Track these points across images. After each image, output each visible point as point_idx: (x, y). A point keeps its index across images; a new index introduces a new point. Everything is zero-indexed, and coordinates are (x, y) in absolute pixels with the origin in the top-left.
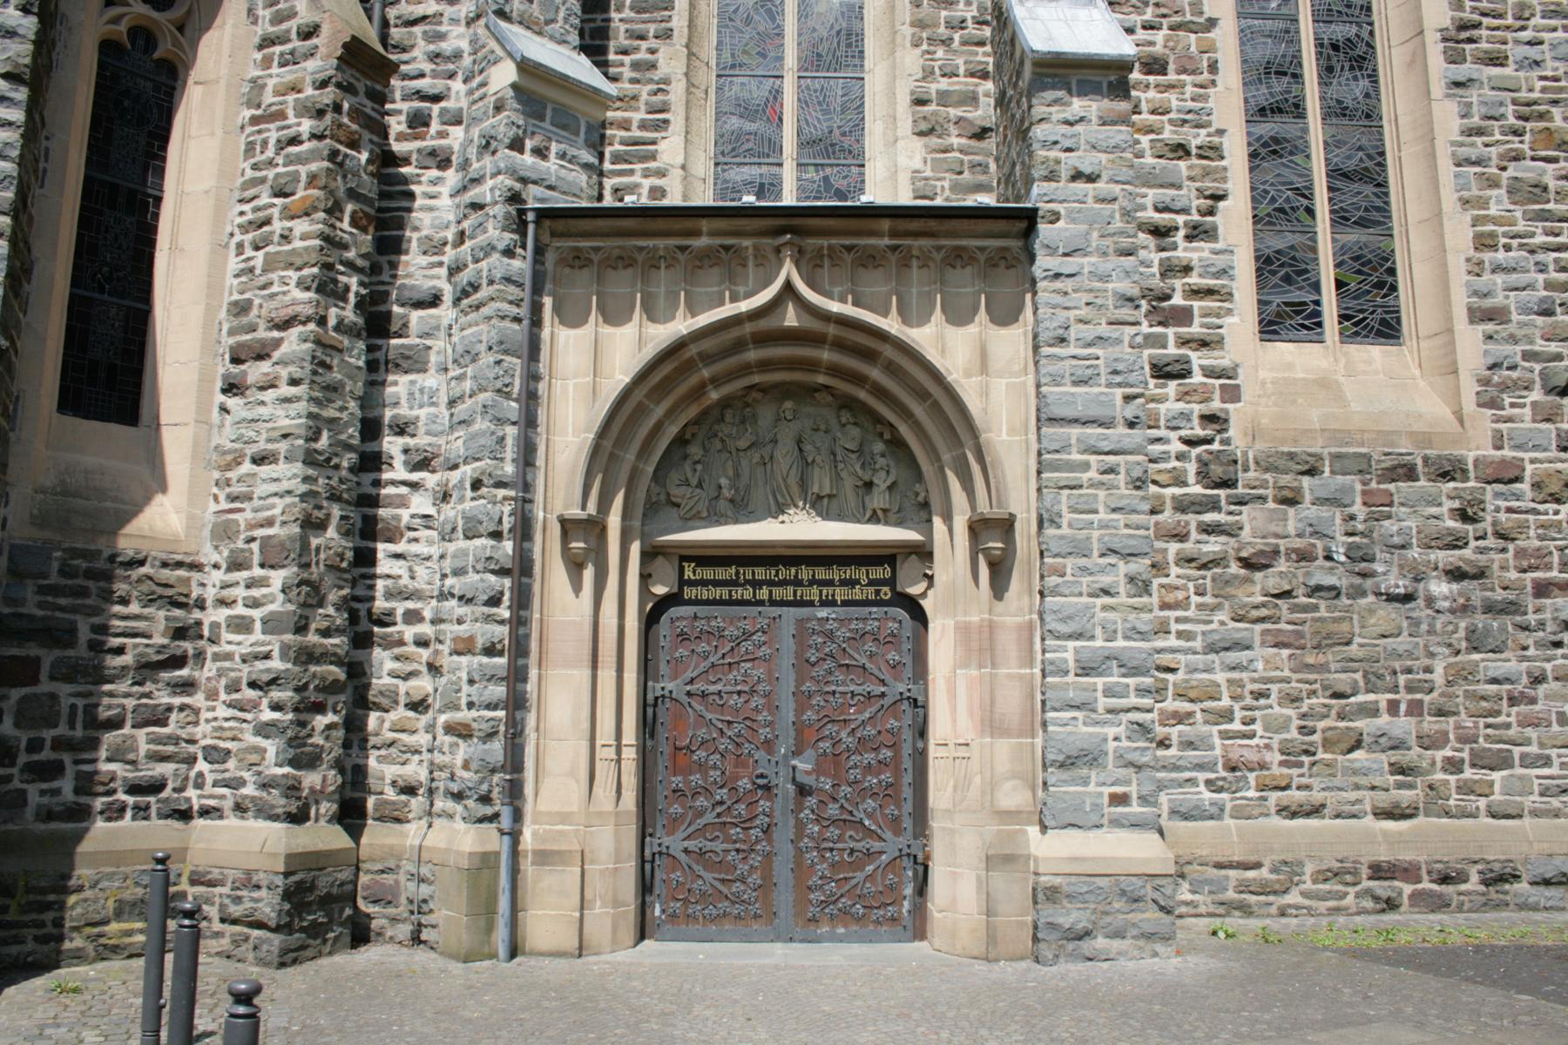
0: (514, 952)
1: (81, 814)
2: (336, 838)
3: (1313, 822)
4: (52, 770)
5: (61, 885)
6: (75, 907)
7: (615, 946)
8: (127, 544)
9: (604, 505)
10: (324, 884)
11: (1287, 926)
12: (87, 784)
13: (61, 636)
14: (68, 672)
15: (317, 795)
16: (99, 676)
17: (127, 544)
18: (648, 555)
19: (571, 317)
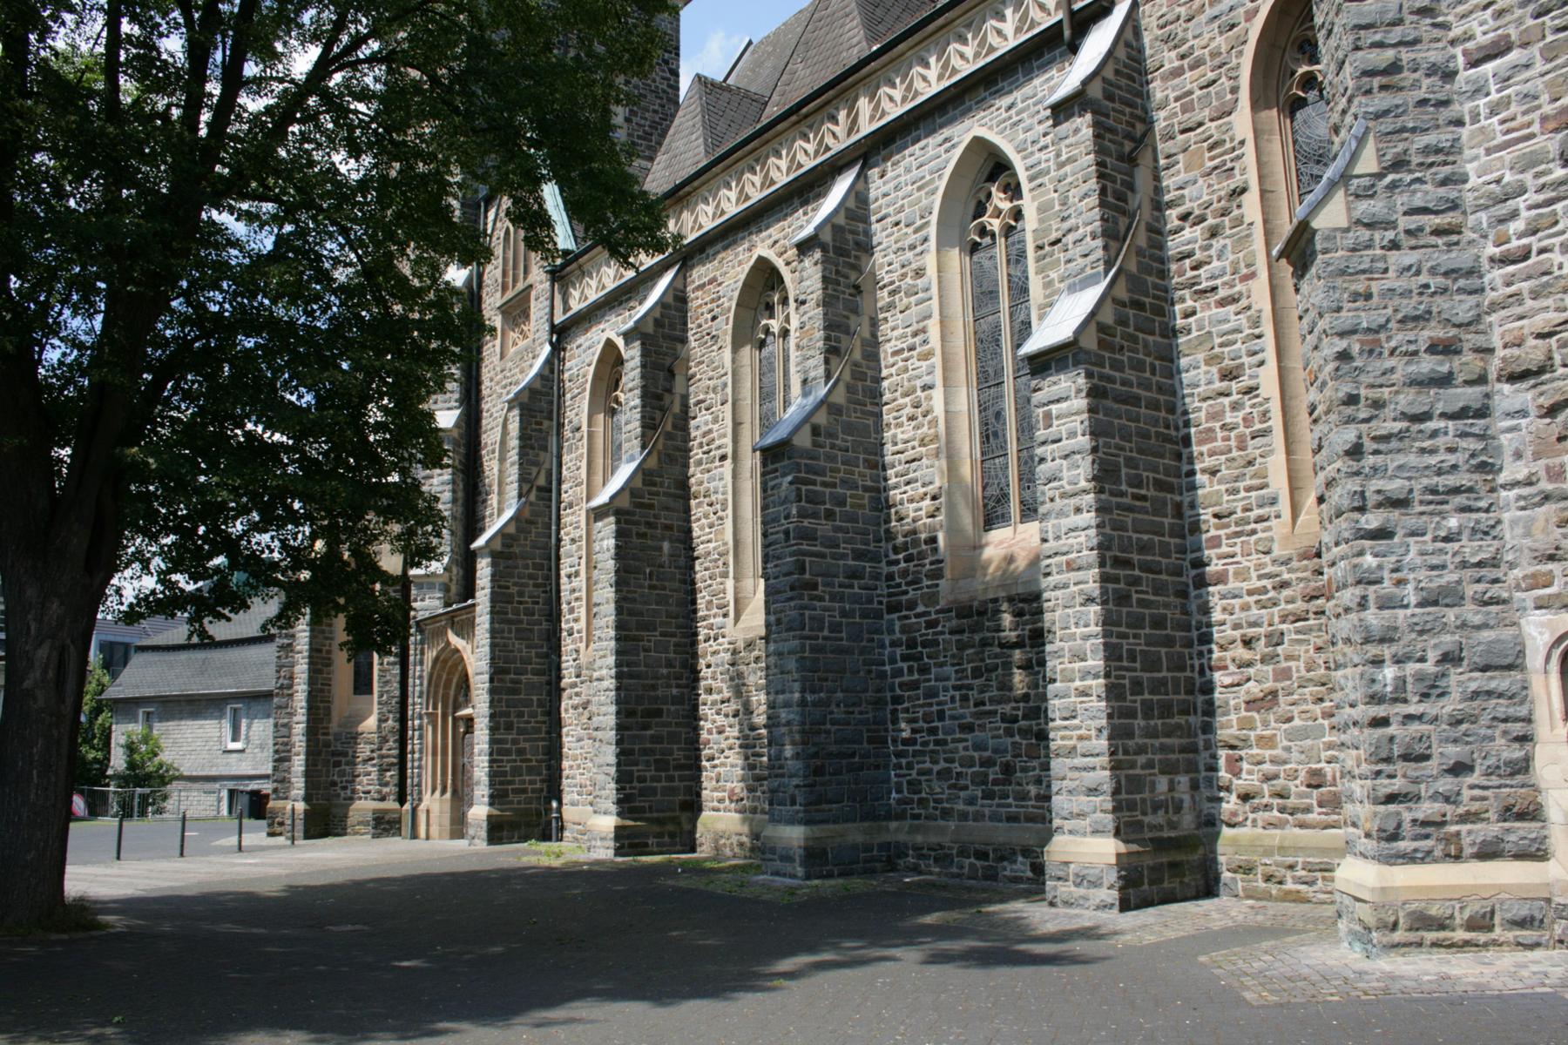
0: (428, 838)
1: (352, 799)
2: (396, 805)
3: (1091, 774)
4: (345, 788)
5: (346, 816)
6: (350, 821)
7: (441, 837)
8: (361, 728)
9: (435, 708)
10: (387, 817)
11: (1273, 837)
12: (354, 791)
13: (345, 754)
14: (347, 764)
15: (389, 794)
16: (355, 764)
17: (361, 728)
18: (455, 720)
19: (251, 717)
